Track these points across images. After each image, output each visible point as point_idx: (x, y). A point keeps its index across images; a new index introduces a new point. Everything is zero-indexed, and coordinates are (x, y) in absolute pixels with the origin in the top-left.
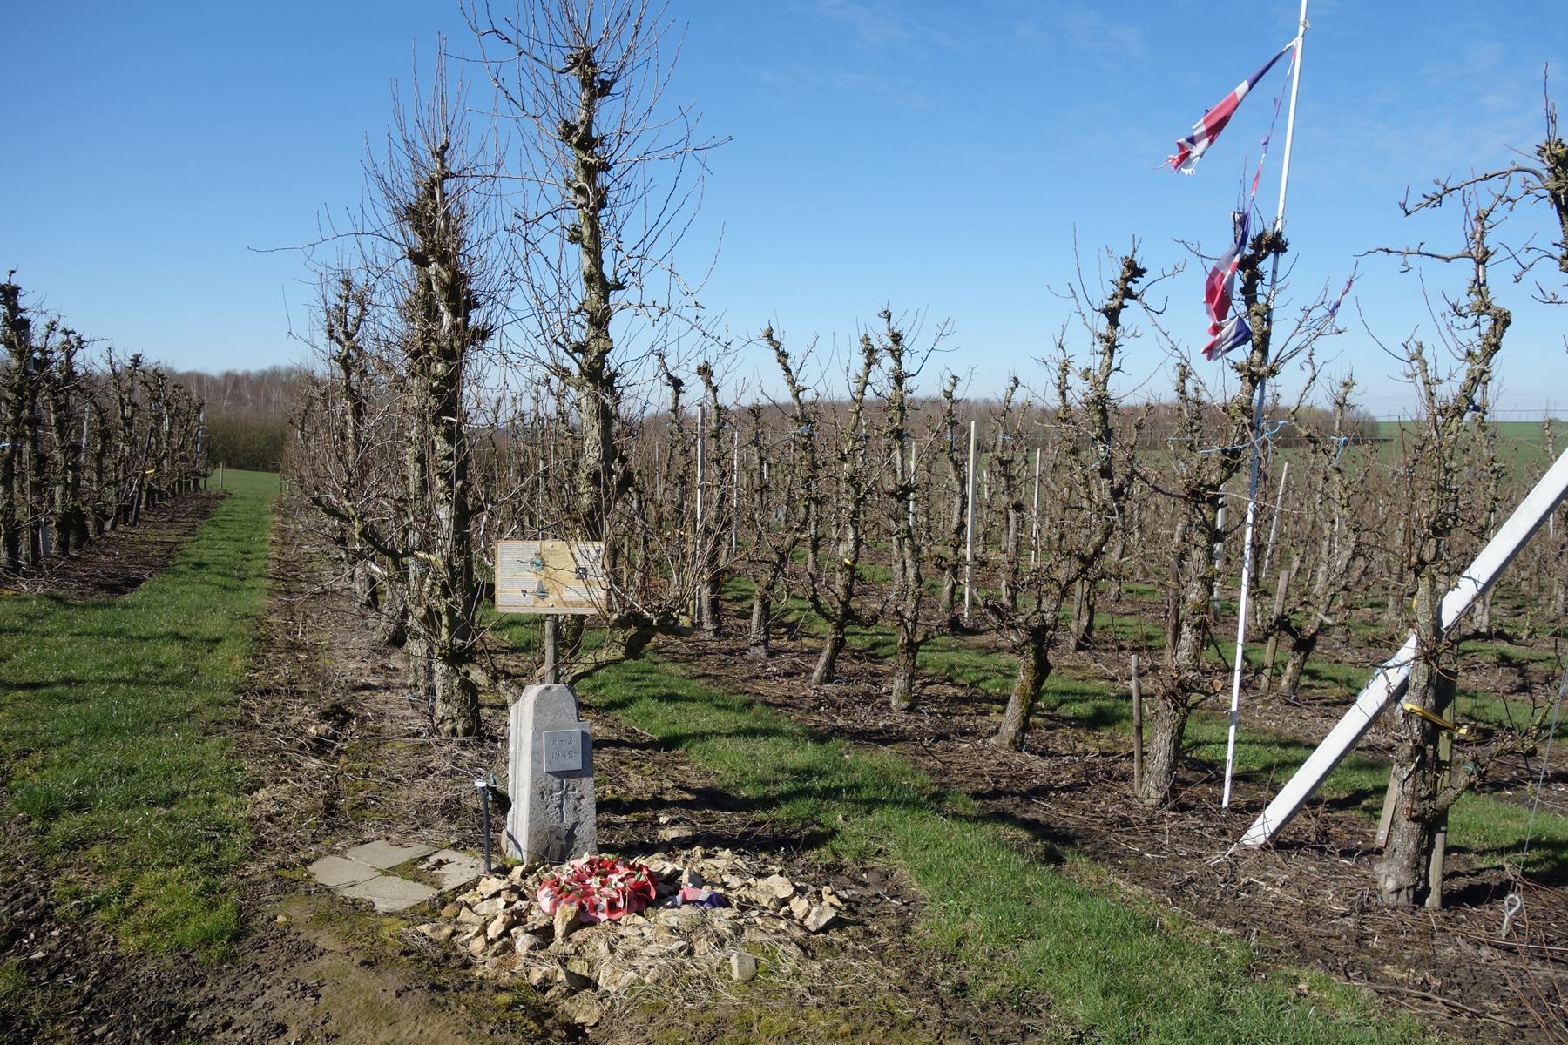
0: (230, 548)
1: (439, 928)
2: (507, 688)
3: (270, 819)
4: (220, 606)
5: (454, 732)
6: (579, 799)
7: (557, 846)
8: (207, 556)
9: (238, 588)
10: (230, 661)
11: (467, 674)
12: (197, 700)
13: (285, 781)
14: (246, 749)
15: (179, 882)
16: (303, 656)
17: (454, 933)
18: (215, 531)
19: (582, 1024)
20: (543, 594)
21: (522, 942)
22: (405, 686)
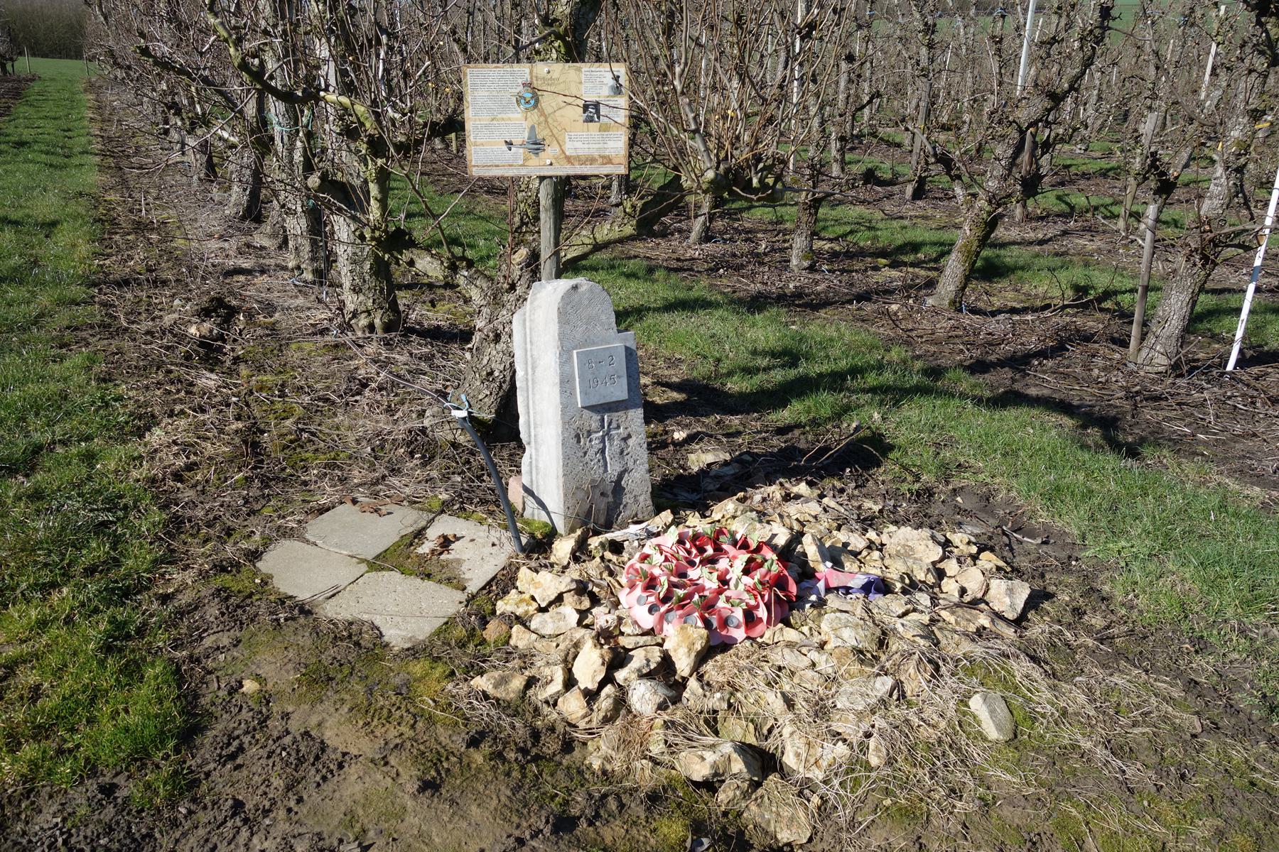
0: (50, 126)
1: (503, 681)
2: (471, 280)
3: (178, 477)
4: (50, 186)
5: (371, 327)
6: (625, 439)
7: (602, 504)
8: (27, 135)
9: (64, 167)
10: (72, 248)
11: (411, 263)
12: (44, 300)
13: (182, 412)
14: (118, 365)
15: (69, 621)
16: (154, 237)
17: (531, 682)
18: (31, 111)
19: (789, 844)
20: (536, 146)
21: (644, 697)
22: (285, 268)
